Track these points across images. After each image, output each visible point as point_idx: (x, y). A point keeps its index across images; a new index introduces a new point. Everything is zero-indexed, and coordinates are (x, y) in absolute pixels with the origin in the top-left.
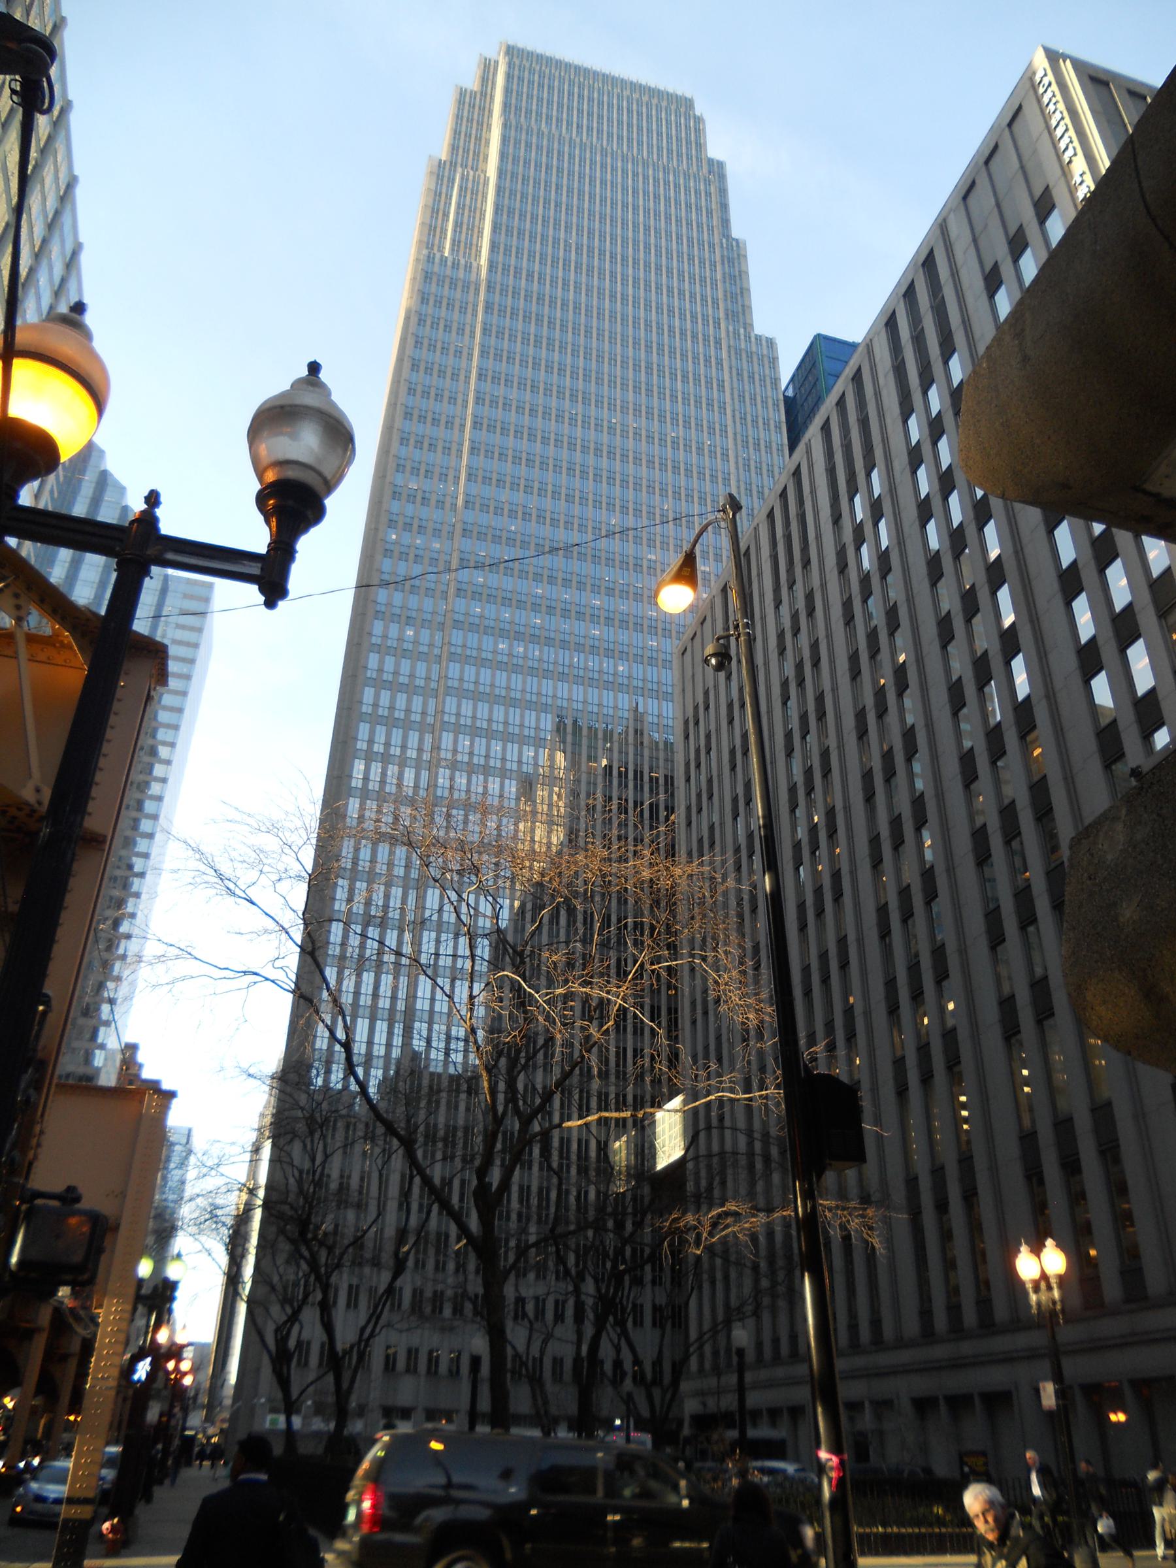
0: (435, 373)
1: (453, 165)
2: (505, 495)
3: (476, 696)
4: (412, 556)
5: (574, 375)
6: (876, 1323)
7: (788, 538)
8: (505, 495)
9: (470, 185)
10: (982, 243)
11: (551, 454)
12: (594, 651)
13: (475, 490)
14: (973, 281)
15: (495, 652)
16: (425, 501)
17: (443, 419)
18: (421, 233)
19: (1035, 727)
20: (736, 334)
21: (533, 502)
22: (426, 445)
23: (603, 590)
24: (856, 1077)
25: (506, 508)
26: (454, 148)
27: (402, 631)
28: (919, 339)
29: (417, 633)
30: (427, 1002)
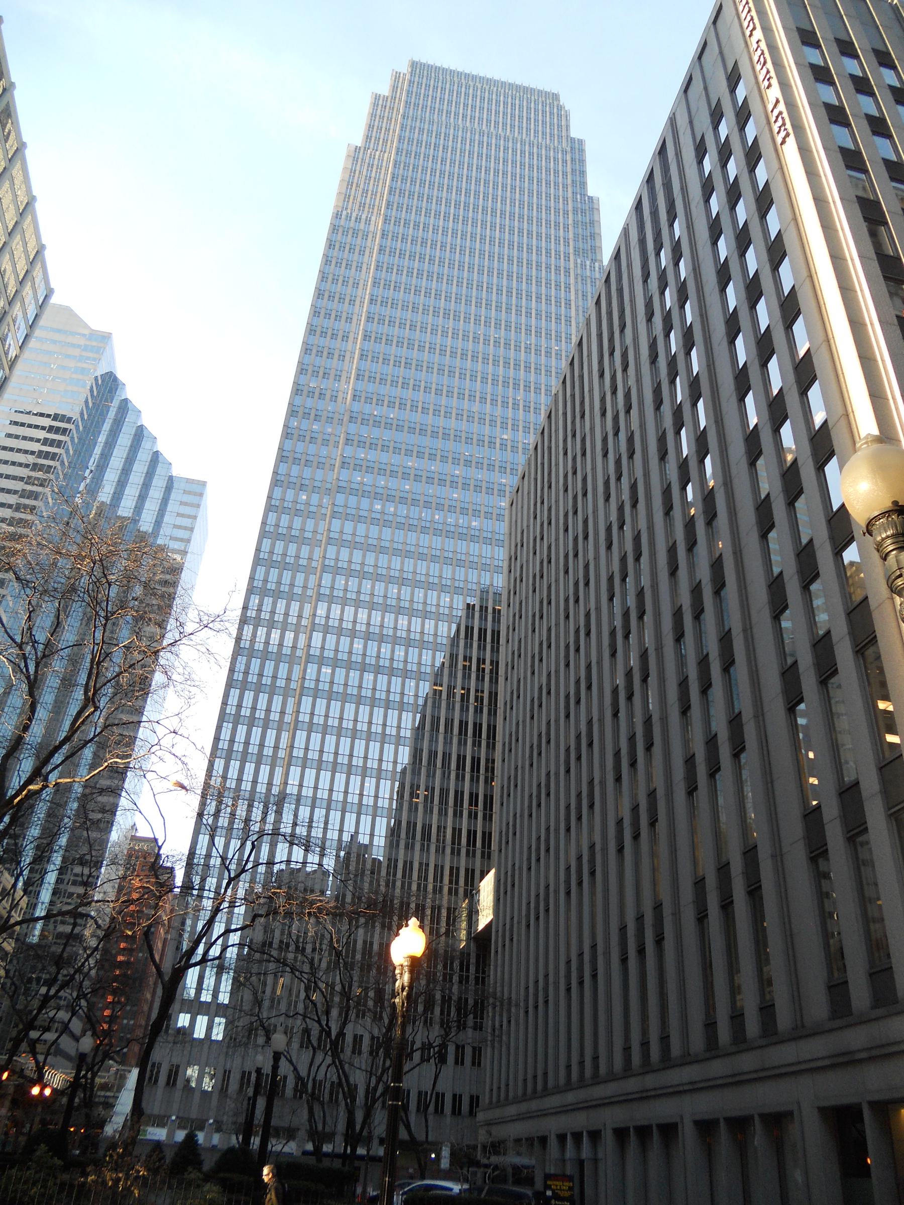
0: (336, 299)
1: (366, 149)
2: (385, 390)
3: (354, 545)
4: (308, 438)
5: (448, 299)
7: (573, 396)
8: (385, 390)
9: (376, 162)
10: (695, 122)
12: (452, 509)
13: (361, 386)
14: (689, 154)
15: (371, 511)
16: (322, 395)
17: (341, 334)
18: (338, 200)
20: (583, 266)
21: (409, 394)
22: (325, 354)
23: (462, 462)
24: (701, 873)
25: (386, 400)
26: (368, 138)
28: (655, 213)
29: (309, 497)
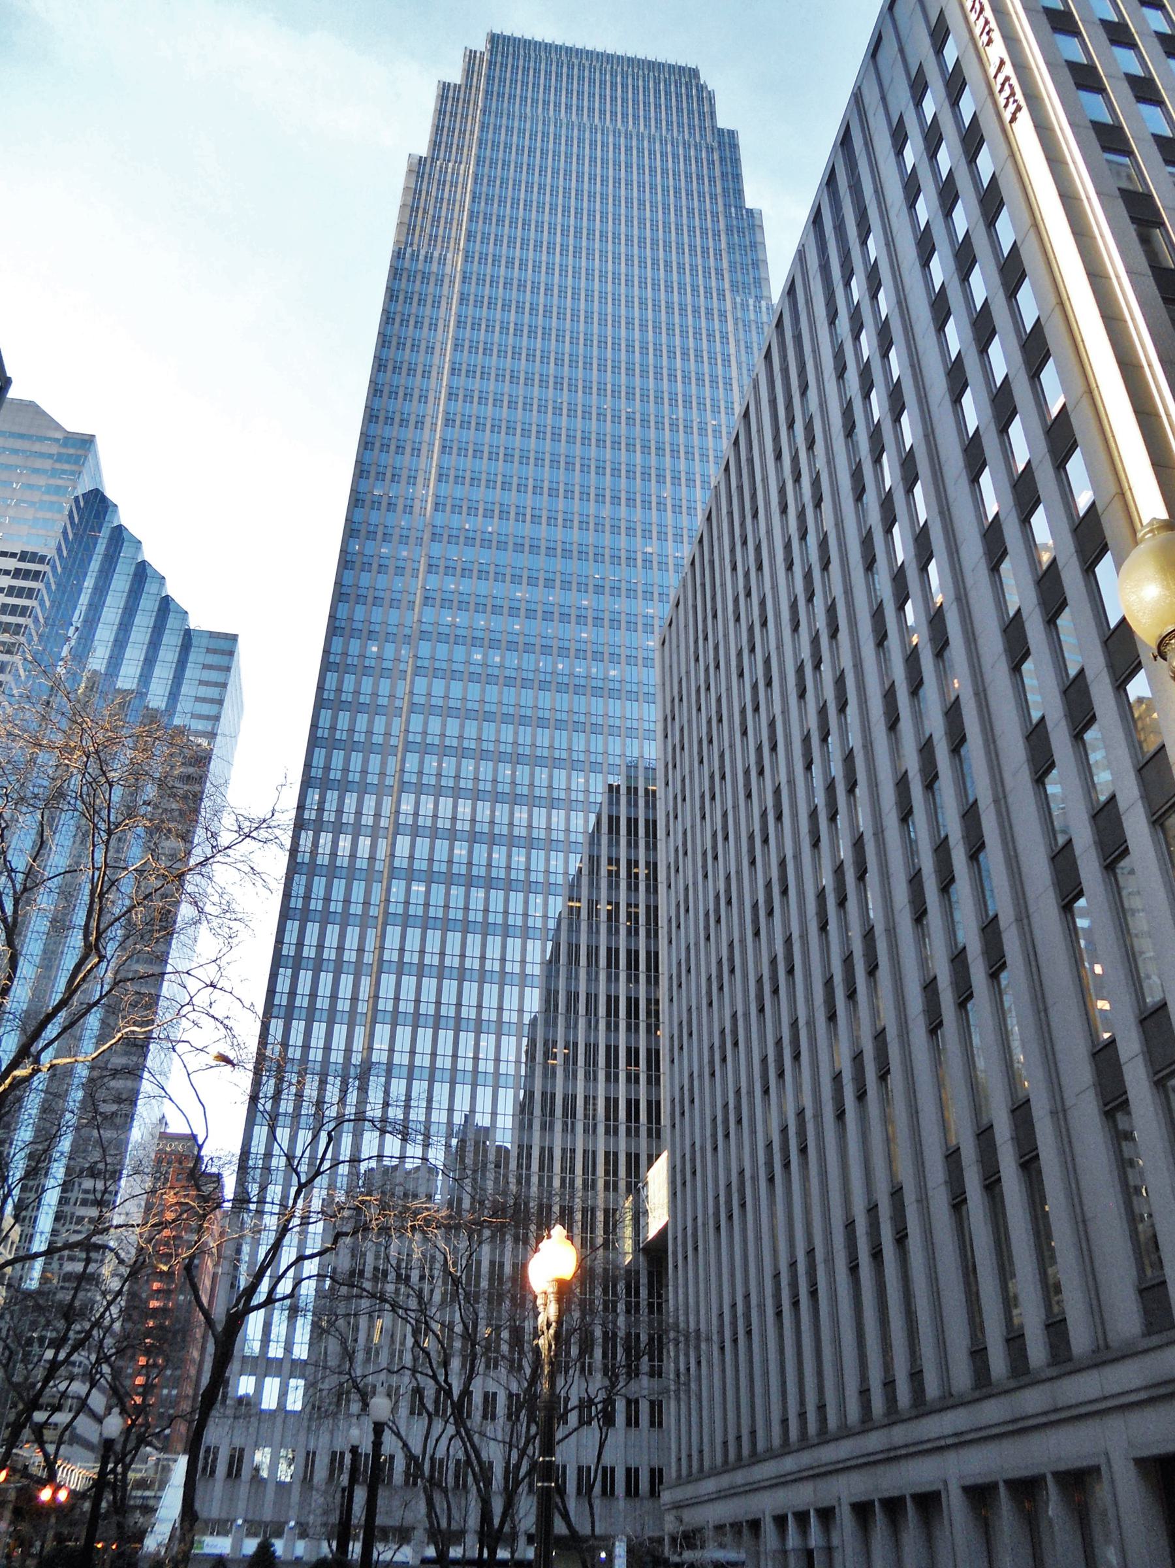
6: (1056, 1327)
11: (623, 545)
15: (468, 662)
19: (1126, 852)
26: (435, 144)
27: (364, 647)
30: (427, 1059)
